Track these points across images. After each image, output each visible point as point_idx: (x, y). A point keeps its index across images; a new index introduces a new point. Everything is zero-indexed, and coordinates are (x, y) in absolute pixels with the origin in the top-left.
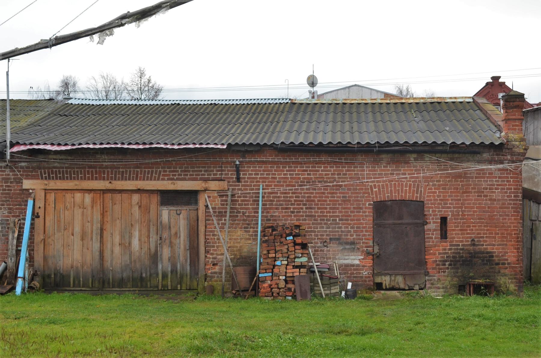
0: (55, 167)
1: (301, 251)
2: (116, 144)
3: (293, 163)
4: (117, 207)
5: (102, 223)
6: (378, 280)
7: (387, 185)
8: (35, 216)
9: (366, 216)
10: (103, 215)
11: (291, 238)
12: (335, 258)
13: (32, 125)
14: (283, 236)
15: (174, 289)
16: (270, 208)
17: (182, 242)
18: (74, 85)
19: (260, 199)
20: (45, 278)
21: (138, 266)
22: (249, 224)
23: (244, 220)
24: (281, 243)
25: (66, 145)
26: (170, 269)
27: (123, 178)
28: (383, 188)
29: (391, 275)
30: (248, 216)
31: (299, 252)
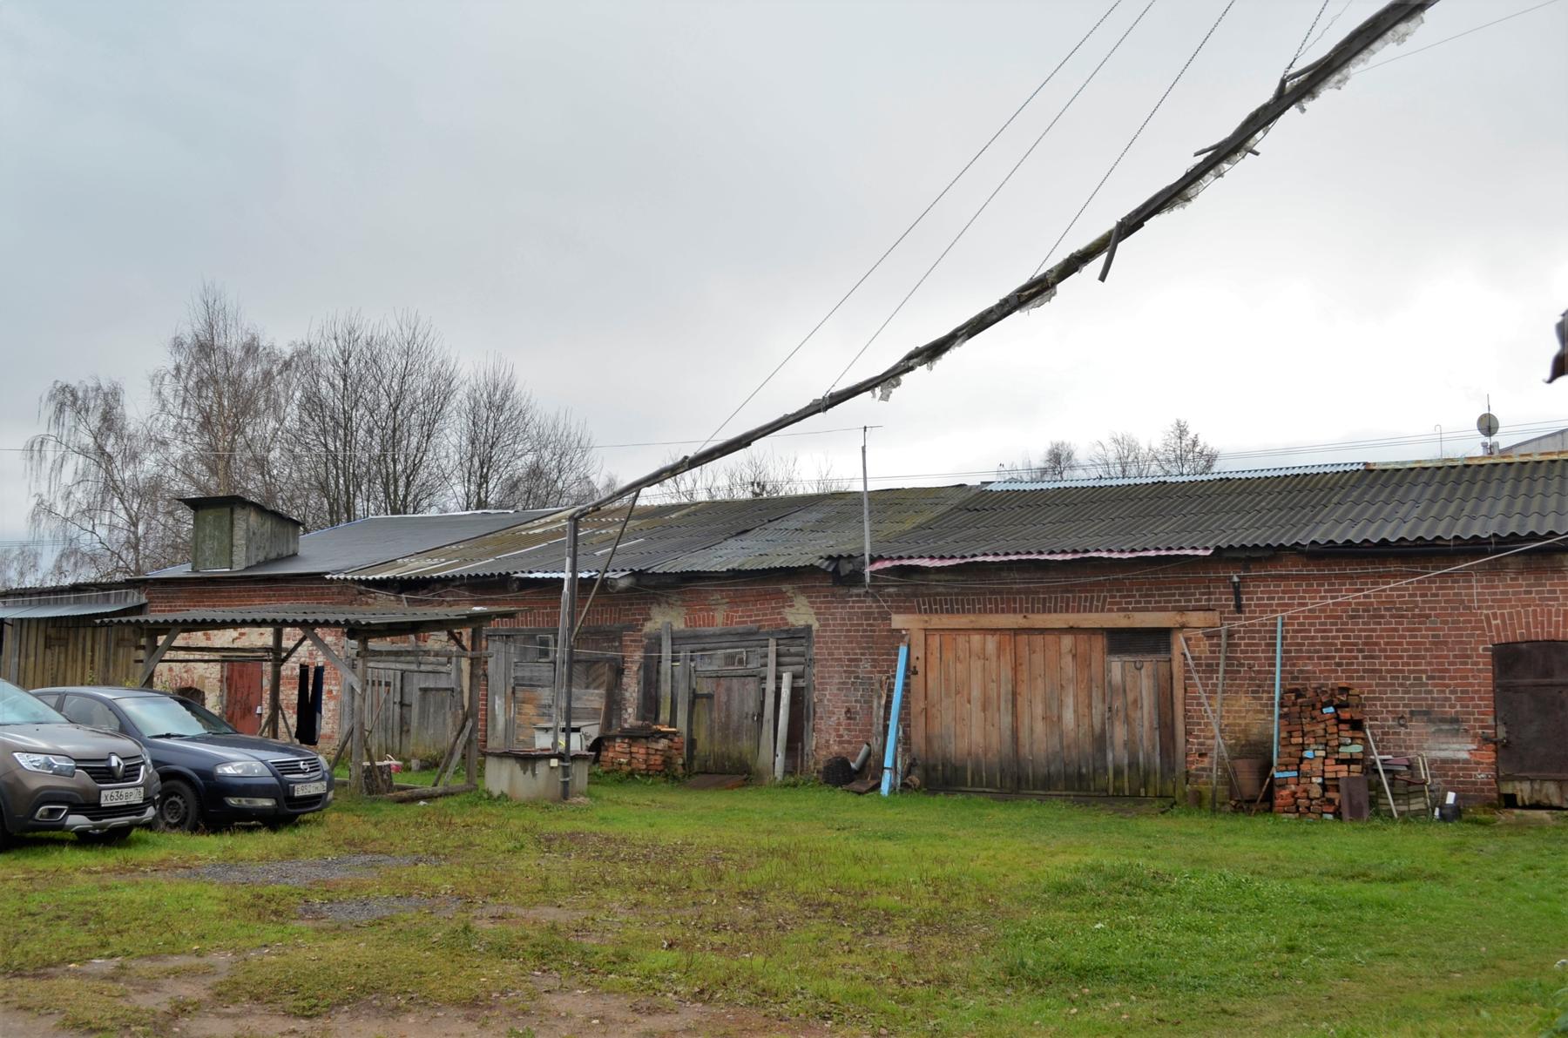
0: (938, 594)
1: (1350, 733)
2: (1029, 553)
3: (1336, 577)
4: (1038, 658)
5: (1015, 682)
6: (1508, 789)
7: (1518, 613)
8: (910, 671)
9: (1479, 671)
10: (1015, 670)
11: (1331, 709)
12: (1420, 748)
13: (920, 527)
14: (1325, 707)
15: (1134, 795)
16: (1298, 658)
17: (1146, 716)
18: (1069, 457)
19: (1279, 641)
20: (928, 770)
21: (1074, 754)
22: (1260, 685)
23: (1251, 679)
24: (1313, 718)
25: (952, 557)
26: (1126, 761)
27: (1046, 610)
28: (1511, 618)
29: (1532, 781)
30: (1259, 672)
31: (1346, 735)
